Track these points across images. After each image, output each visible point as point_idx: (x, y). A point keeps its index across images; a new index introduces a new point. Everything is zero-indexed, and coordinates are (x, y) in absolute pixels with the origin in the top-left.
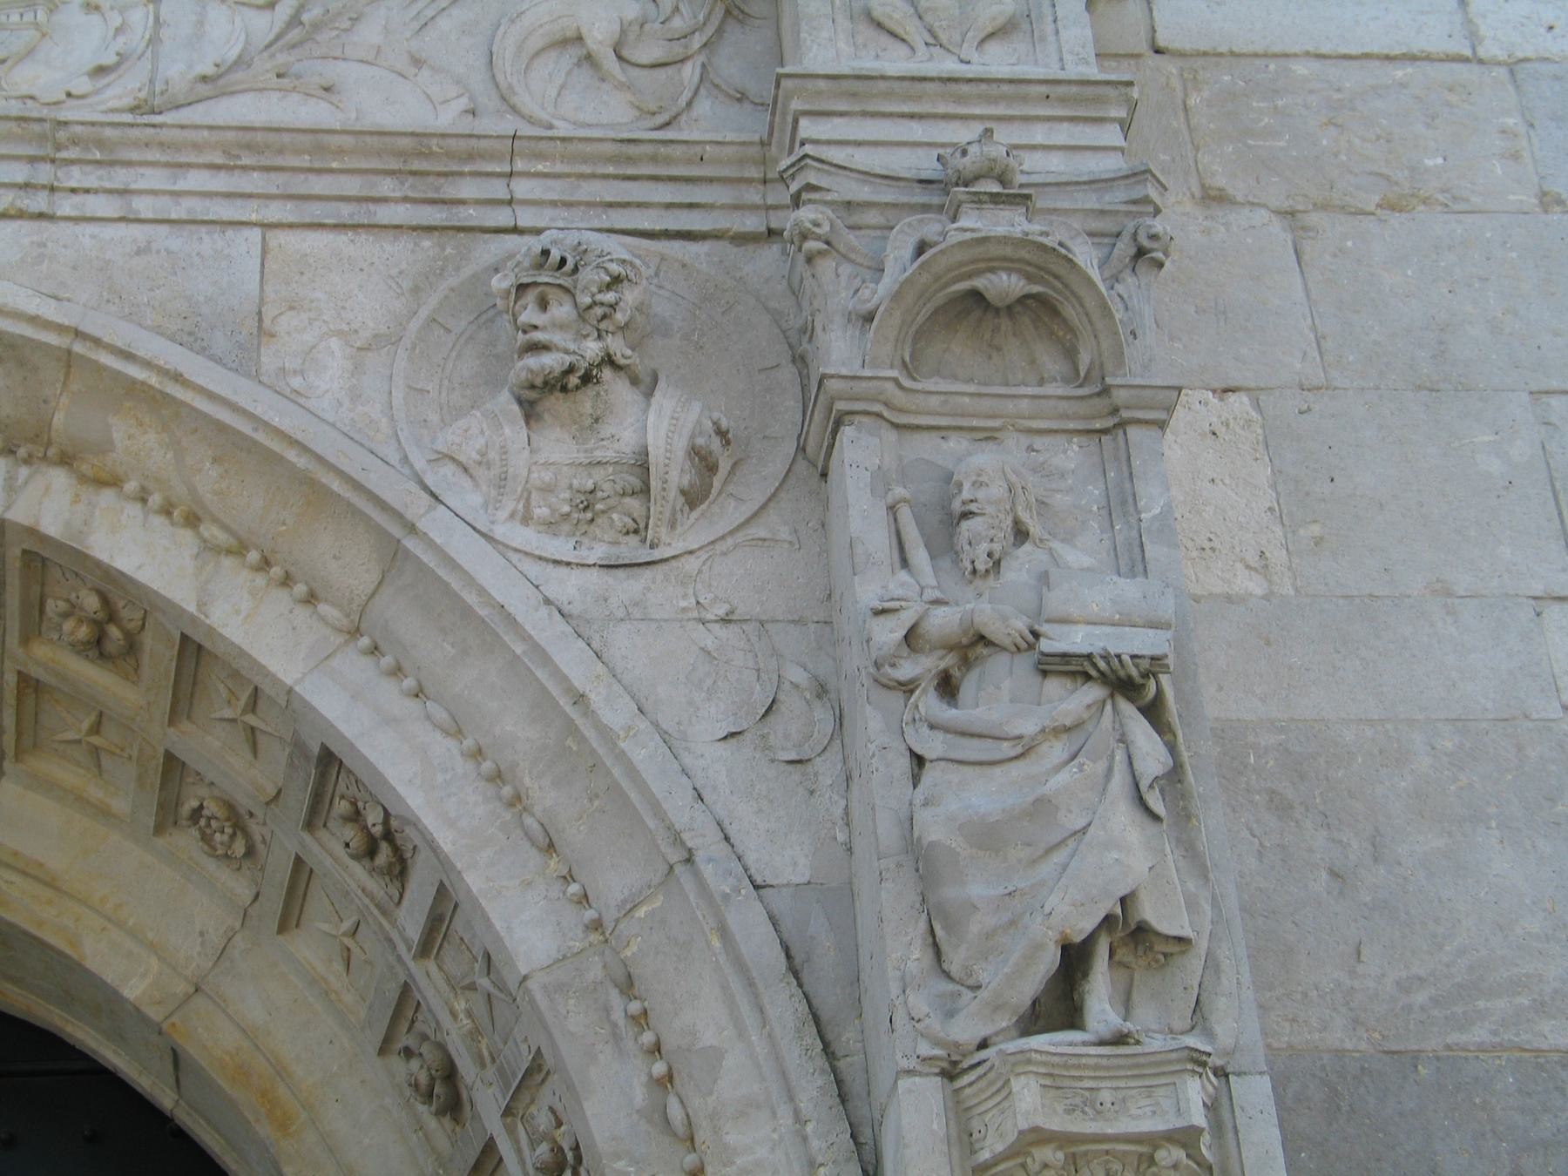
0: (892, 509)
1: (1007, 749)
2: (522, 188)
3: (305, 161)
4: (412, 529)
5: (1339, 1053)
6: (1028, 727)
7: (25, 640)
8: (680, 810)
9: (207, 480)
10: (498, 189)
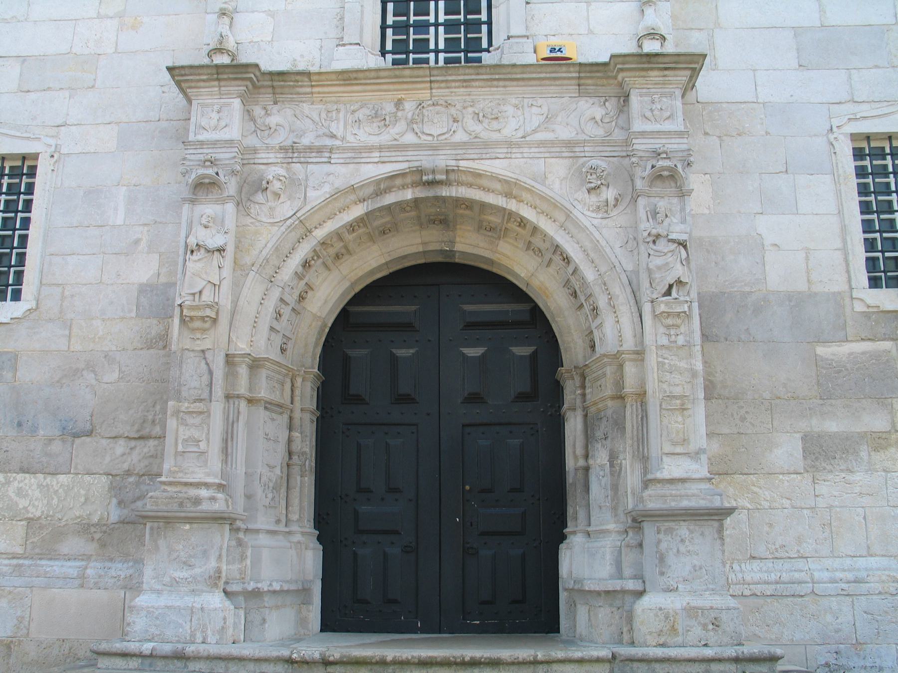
0: (647, 212)
1: (662, 254)
2: (586, 149)
3: (550, 145)
4: (571, 212)
5: (713, 292)
6: (666, 251)
7: (507, 223)
8: (613, 259)
9: (538, 202)
10: (582, 149)
